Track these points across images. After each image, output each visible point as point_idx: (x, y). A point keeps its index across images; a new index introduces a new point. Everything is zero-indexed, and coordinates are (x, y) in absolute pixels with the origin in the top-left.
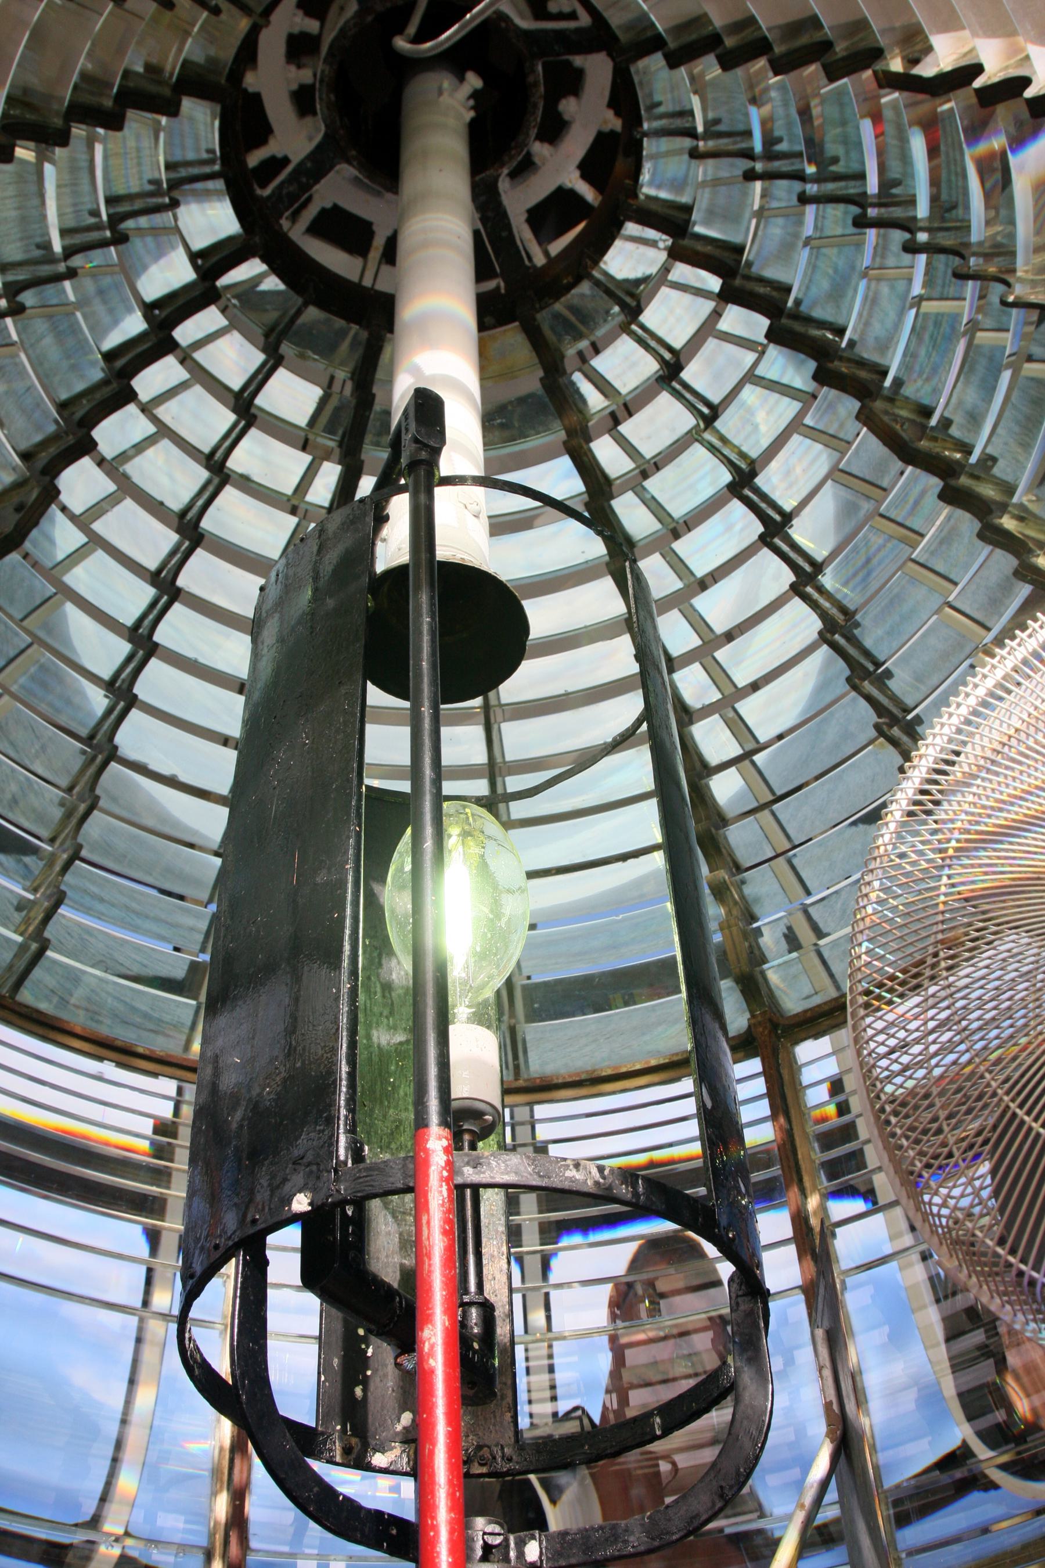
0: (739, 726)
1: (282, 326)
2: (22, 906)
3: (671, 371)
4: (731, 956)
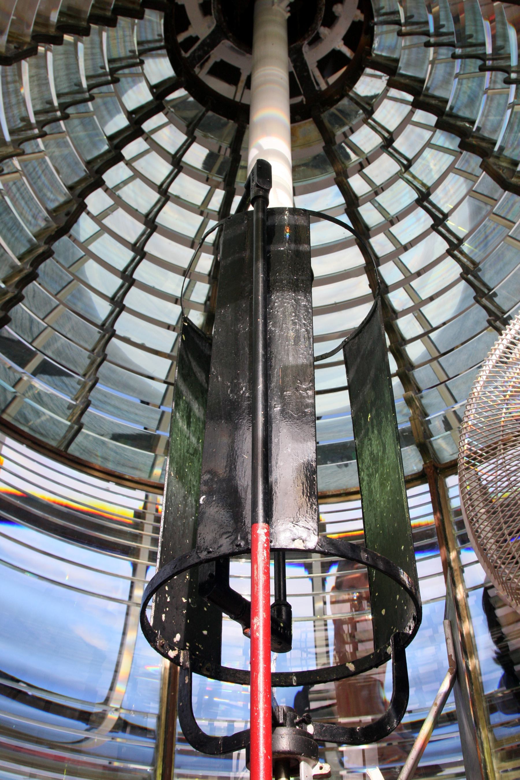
0: (422, 319)
1: (195, 122)
2: (70, 407)
3: (388, 143)
4: (415, 434)
